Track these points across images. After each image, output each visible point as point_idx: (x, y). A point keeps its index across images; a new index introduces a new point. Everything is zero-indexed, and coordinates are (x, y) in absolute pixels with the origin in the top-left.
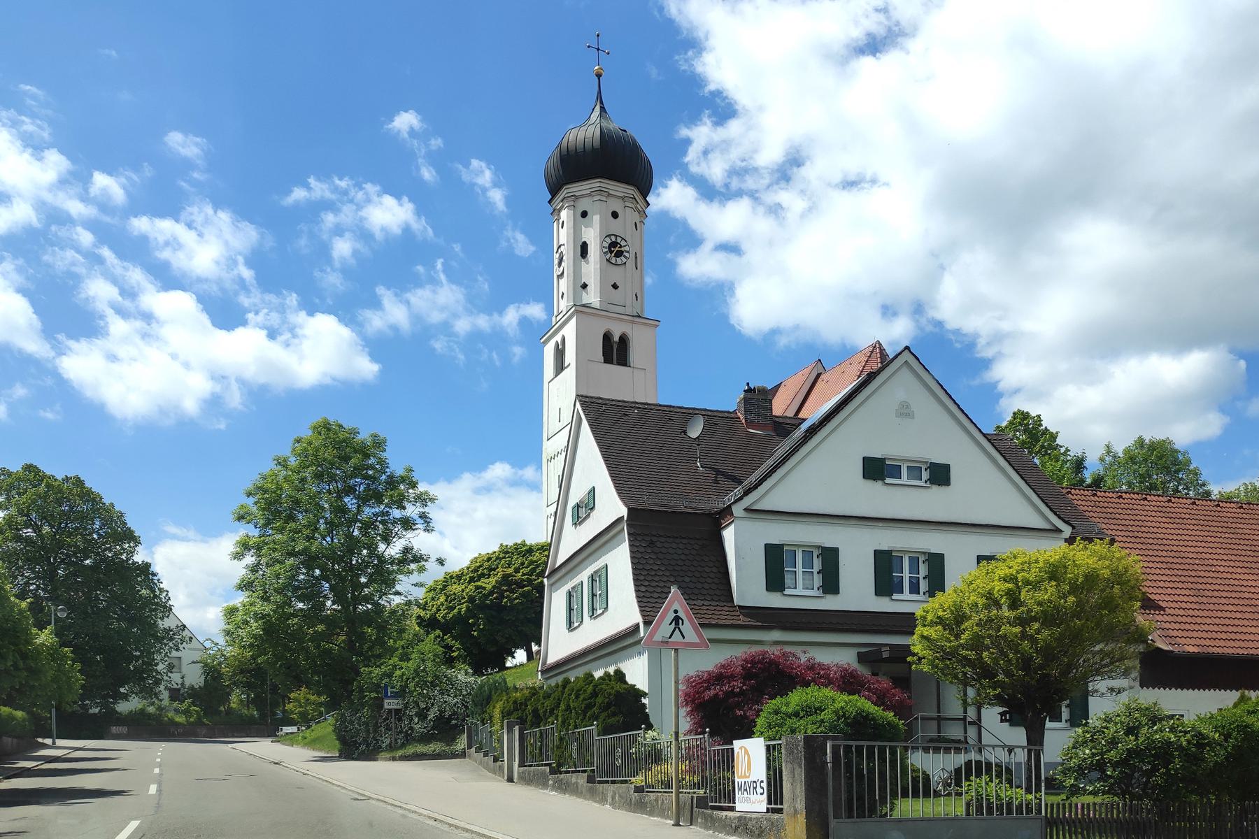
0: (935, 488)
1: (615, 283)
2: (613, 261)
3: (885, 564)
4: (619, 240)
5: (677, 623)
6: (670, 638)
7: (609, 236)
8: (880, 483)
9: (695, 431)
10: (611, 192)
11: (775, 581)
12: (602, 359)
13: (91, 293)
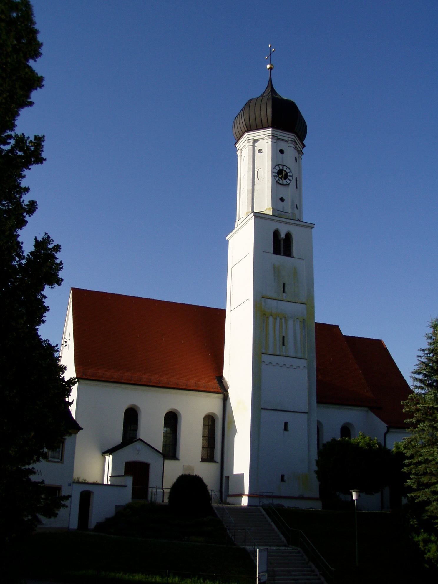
1: (282, 197)
2: (280, 182)
4: (285, 168)
7: (278, 165)
9: (281, 128)
10: (280, 137)
12: (272, 252)
13: (63, 495)
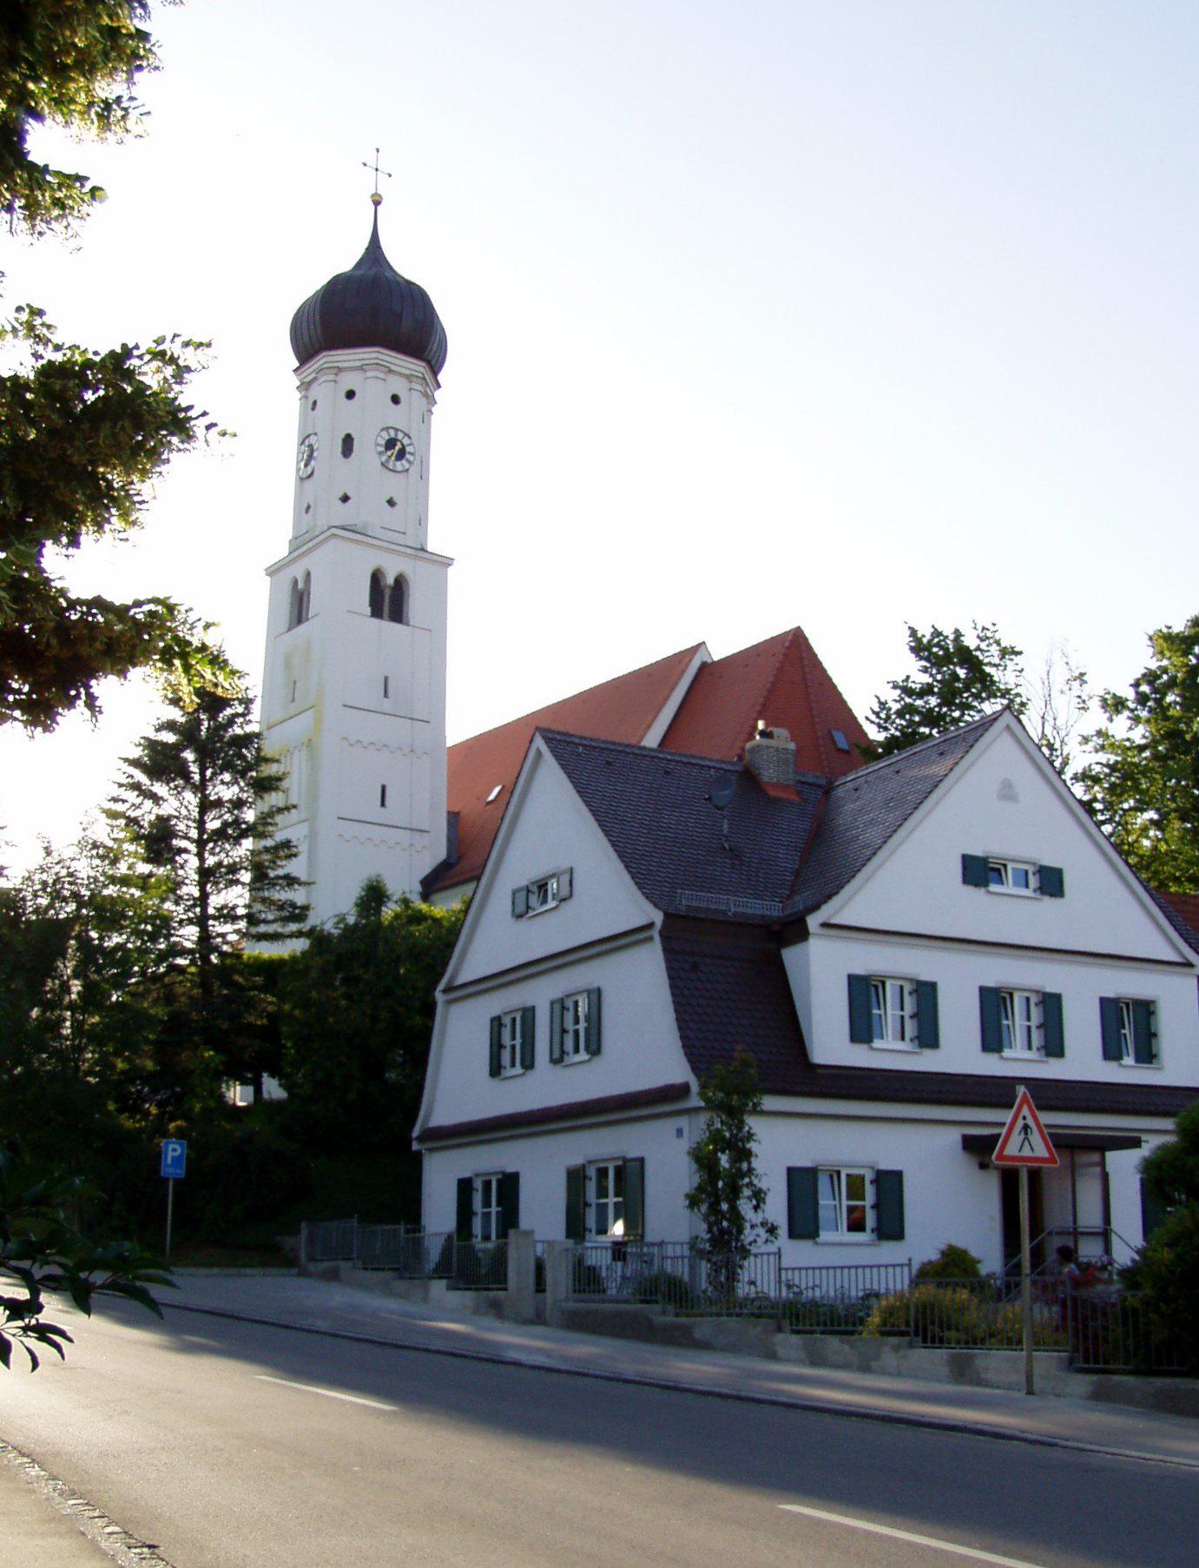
0: (1047, 899)
3: (994, 1003)
4: (400, 436)
5: (1026, 1134)
6: (1020, 1150)
7: (387, 429)
8: (983, 890)
10: (393, 368)
11: (862, 1029)
12: (368, 610)
